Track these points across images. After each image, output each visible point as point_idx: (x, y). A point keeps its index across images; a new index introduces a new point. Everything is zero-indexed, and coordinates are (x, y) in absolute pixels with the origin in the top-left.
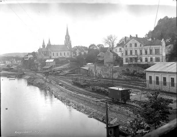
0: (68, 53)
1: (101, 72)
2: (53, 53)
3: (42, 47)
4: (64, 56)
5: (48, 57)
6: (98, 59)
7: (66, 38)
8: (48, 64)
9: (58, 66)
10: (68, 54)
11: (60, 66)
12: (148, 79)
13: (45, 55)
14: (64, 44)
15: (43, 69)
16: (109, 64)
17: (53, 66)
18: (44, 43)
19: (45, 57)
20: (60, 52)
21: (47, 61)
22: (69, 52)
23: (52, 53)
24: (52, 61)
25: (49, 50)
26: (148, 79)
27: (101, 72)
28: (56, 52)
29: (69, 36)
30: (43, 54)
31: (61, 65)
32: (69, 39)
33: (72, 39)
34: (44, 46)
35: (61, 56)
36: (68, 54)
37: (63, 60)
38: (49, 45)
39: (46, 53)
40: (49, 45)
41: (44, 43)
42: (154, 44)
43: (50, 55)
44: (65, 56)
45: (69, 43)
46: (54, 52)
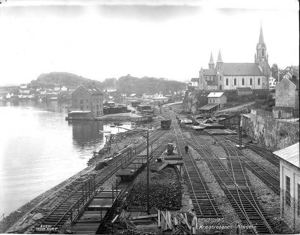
0: (259, 80)
1: (264, 130)
2: (227, 80)
3: (207, 68)
4: (249, 86)
5: (216, 88)
6: (272, 96)
7: (258, 50)
8: (212, 101)
9: (231, 106)
10: (259, 82)
11: (236, 105)
12: (283, 187)
13: (210, 83)
14: (254, 62)
15: (201, 110)
16: (280, 111)
17: (221, 106)
18: (211, 59)
19: (209, 88)
20: (241, 78)
21: (211, 95)
22: (261, 77)
23: (225, 78)
24: (219, 94)
25: (218, 73)
26: (283, 187)
27: (263, 131)
28: (234, 77)
29: (264, 45)
30: (206, 81)
31: (236, 103)
32: (263, 50)
33: (268, 51)
34: (211, 65)
35: (243, 86)
36: (259, 82)
37: (247, 93)
38: (220, 63)
39: (212, 80)
40: (220, 63)
41: (211, 59)
42: (11, 88)
43: (220, 82)
44: (251, 87)
45: (263, 60)
46: (229, 78)
